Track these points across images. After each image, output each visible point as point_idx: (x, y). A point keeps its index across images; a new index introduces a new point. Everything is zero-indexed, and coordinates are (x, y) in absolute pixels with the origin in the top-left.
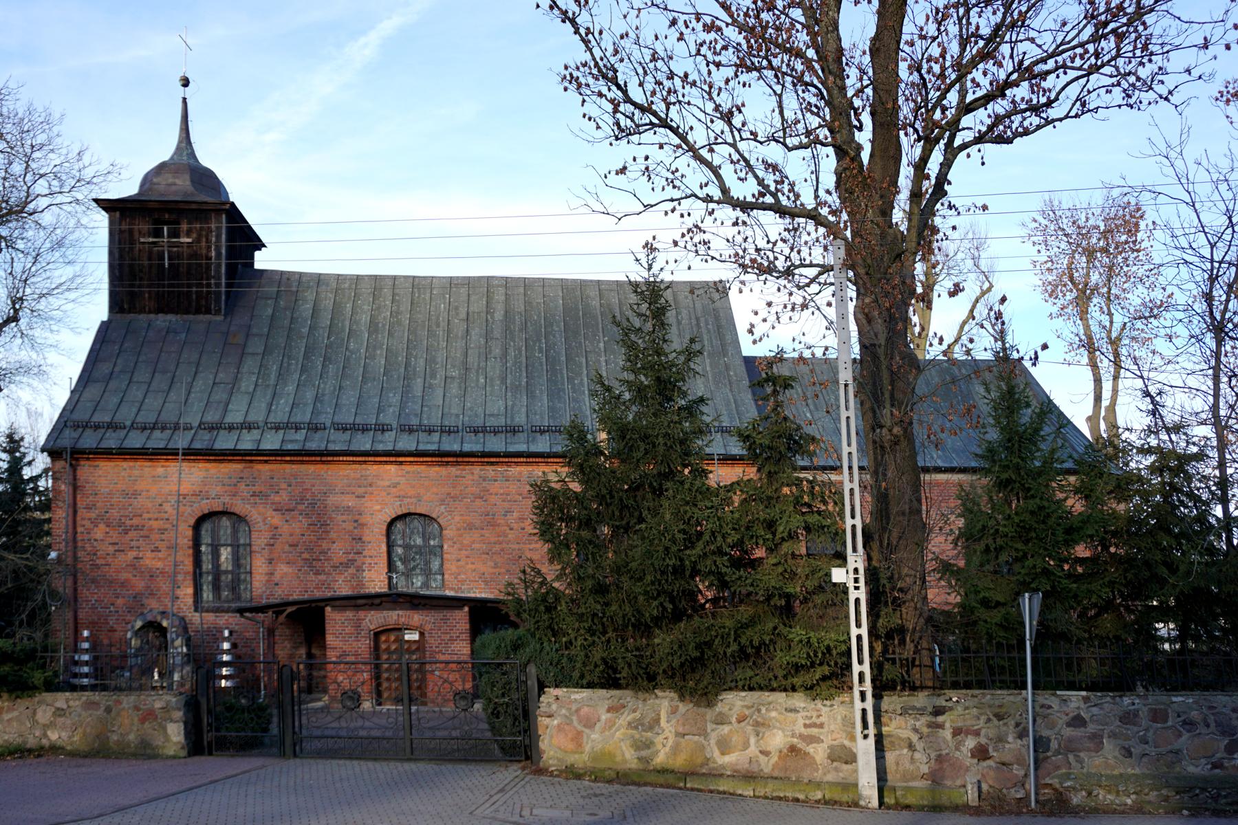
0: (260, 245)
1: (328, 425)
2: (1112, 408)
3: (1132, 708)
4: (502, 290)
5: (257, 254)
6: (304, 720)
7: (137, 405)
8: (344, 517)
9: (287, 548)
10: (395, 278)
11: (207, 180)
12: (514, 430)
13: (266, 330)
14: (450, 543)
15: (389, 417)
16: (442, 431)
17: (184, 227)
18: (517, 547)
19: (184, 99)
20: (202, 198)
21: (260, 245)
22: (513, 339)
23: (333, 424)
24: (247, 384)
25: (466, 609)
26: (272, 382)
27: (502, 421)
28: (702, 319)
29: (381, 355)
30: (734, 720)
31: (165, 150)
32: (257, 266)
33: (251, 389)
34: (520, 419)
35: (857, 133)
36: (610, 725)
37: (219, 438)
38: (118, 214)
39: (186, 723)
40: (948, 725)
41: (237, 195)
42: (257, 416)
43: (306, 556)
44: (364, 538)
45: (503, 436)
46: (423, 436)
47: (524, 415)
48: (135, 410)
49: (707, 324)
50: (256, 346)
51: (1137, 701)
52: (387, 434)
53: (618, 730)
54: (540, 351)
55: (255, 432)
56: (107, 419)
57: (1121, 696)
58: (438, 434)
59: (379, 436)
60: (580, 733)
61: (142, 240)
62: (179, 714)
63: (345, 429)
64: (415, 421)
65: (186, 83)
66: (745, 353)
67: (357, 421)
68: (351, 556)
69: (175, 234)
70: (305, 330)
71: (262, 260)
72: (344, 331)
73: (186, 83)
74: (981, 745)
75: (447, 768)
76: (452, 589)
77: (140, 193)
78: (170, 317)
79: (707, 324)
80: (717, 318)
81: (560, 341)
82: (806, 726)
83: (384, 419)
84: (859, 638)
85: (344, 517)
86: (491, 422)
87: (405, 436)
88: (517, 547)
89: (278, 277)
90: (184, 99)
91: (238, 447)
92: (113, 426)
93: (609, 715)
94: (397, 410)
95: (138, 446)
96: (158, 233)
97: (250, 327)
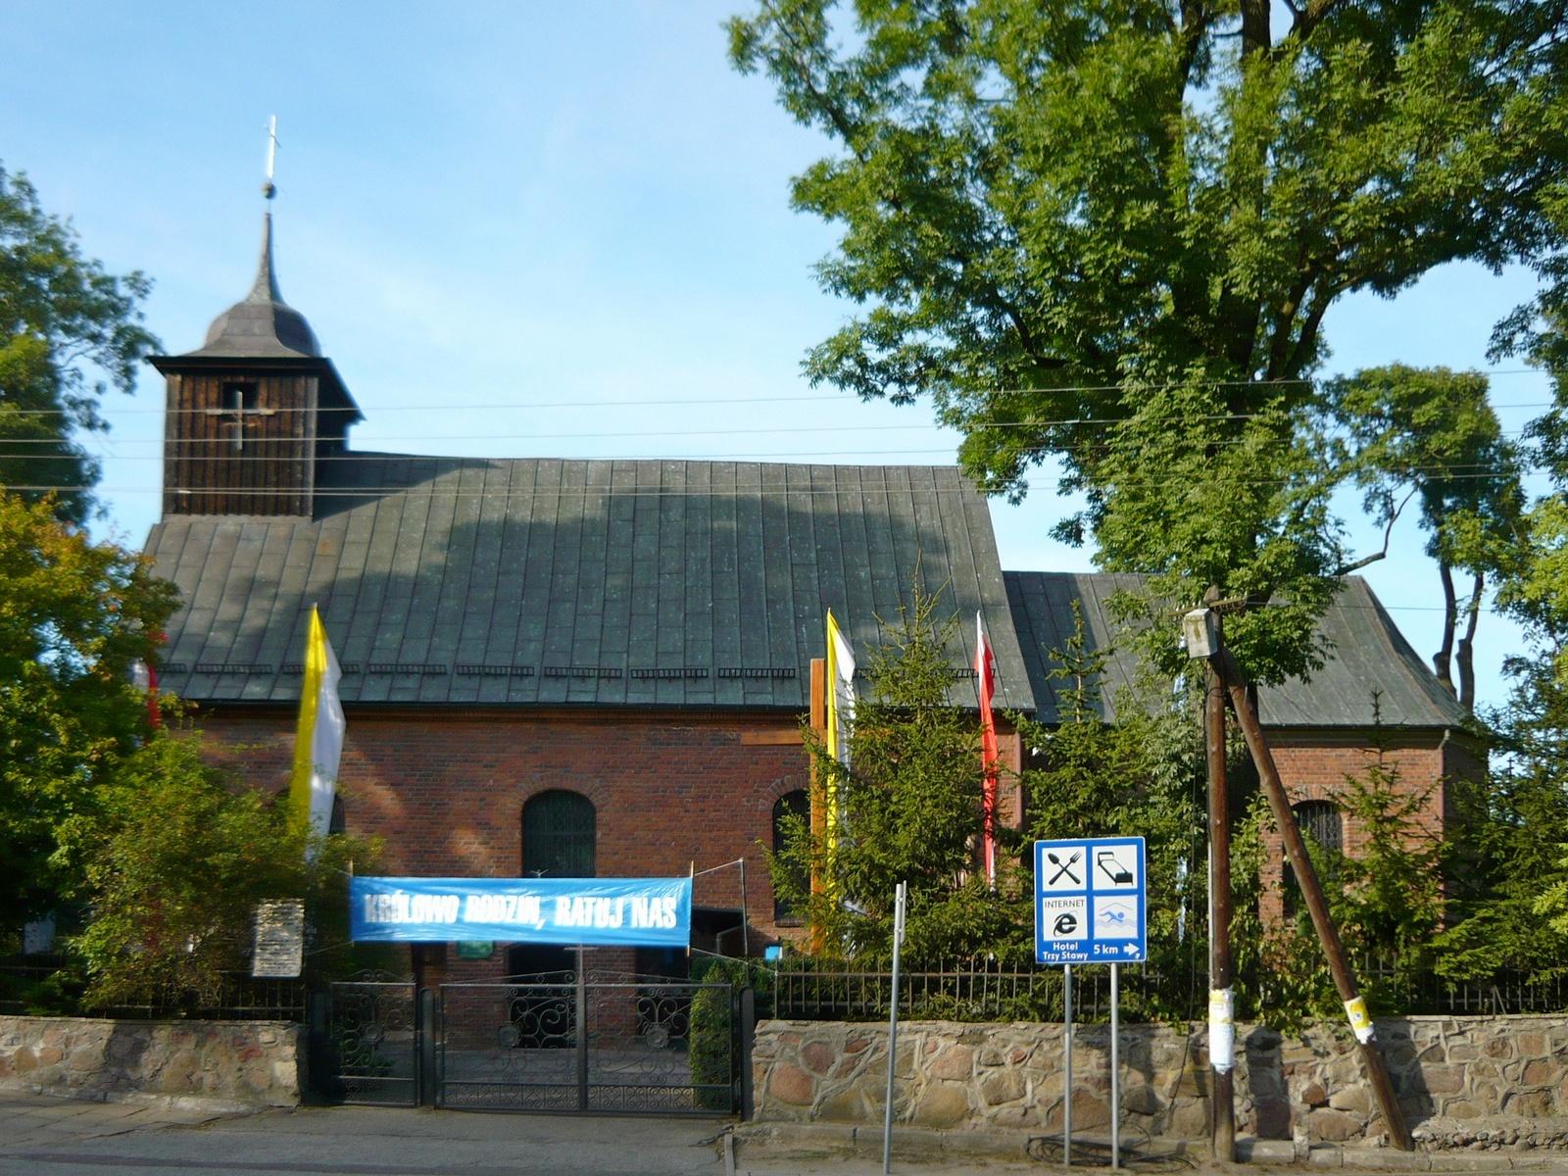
0: (354, 416)
1: (449, 669)
2: (1466, 646)
10: (537, 461)
11: (291, 327)
12: (695, 676)
15: (529, 656)
16: (599, 677)
17: (263, 393)
20: (291, 353)
21: (354, 416)
23: (456, 666)
28: (948, 520)
30: (1008, 1061)
31: (239, 285)
33: (347, 618)
34: (703, 659)
38: (179, 378)
39: (298, 1062)
41: (330, 346)
44: (493, 823)
45: (681, 683)
46: (576, 685)
47: (708, 654)
49: (954, 526)
52: (526, 681)
55: (355, 677)
60: (807, 1079)
62: (290, 1050)
63: (470, 675)
64: (562, 662)
65: (271, 192)
66: (1006, 566)
69: (249, 402)
70: (418, 536)
73: (271, 192)
77: (205, 348)
78: (244, 518)
79: (954, 526)
80: (968, 518)
83: (523, 659)
86: (666, 664)
87: (551, 683)
91: (273, 697)
93: (847, 1055)
95: (233, 697)
96: (228, 402)
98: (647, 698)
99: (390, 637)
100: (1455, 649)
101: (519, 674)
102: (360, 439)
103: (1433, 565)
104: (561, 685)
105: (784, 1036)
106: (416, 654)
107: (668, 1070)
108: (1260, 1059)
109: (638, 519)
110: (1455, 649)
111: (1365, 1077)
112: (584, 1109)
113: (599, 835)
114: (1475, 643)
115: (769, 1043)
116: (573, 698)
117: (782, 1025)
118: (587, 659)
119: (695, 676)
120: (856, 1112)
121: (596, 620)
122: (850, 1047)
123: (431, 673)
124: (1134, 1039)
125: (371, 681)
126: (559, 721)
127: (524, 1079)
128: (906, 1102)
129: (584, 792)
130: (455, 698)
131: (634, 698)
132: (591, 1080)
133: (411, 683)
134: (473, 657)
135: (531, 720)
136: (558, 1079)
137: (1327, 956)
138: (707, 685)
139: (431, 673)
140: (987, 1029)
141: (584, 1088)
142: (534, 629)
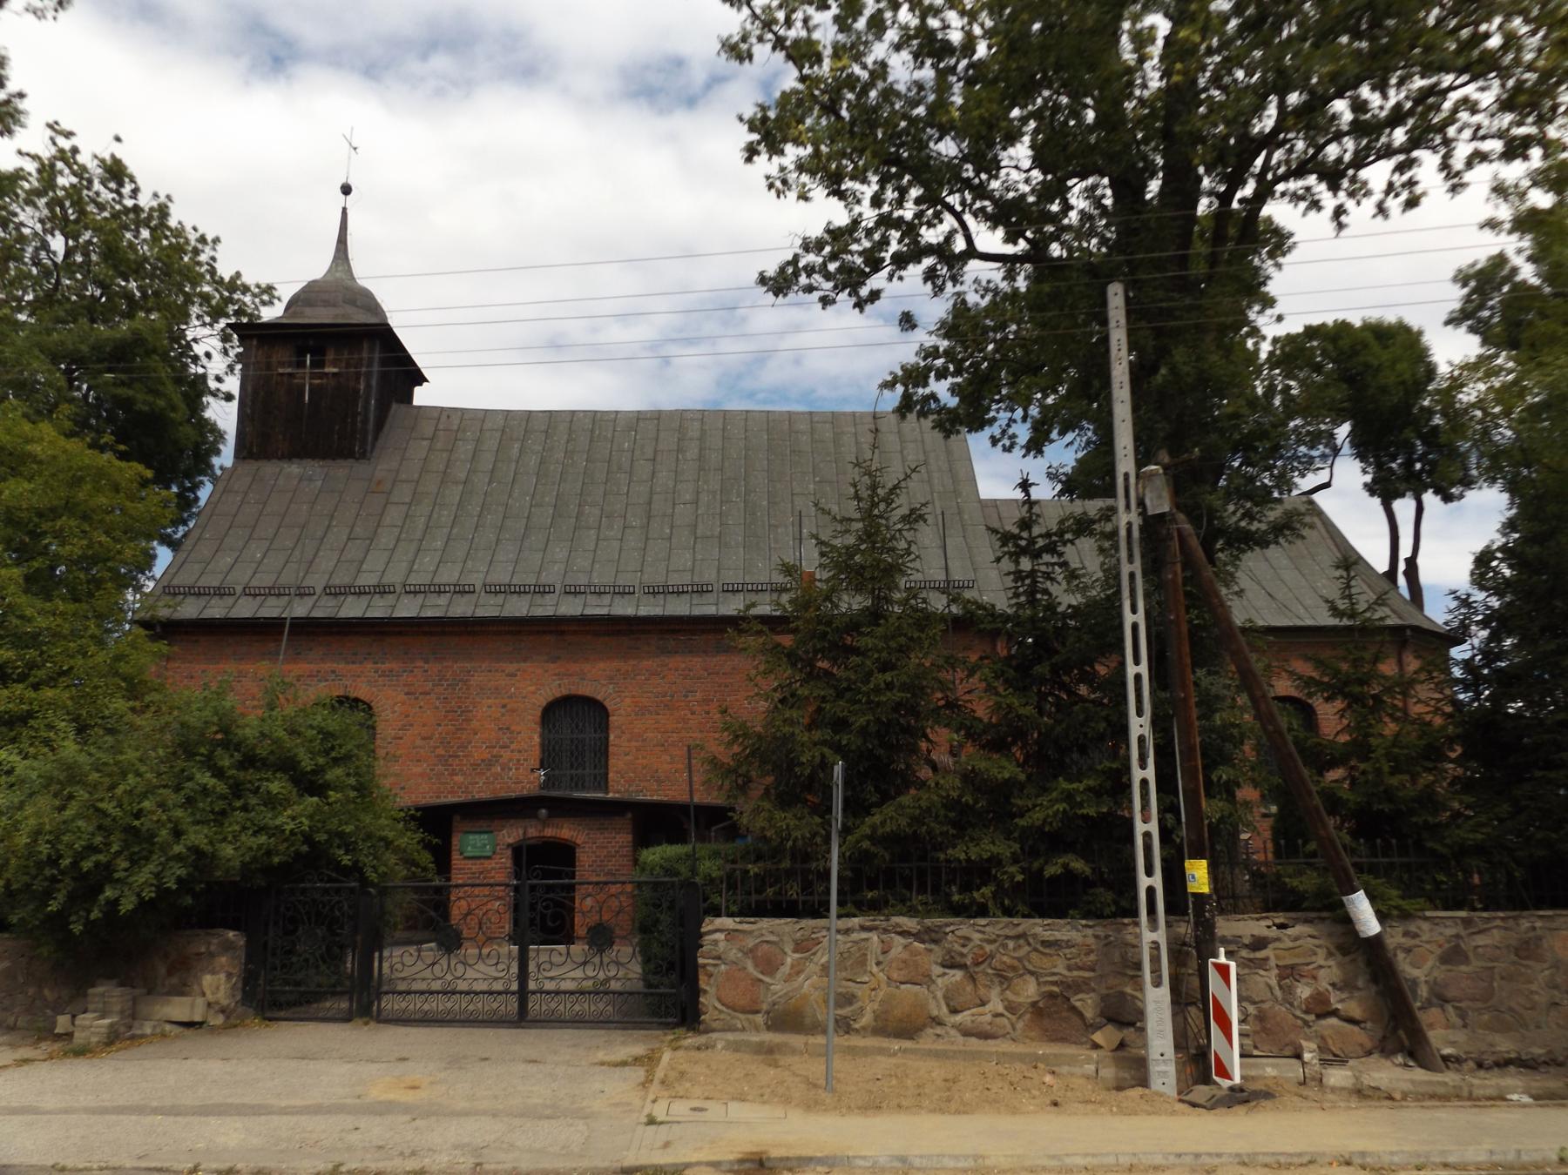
0: (420, 379)
2: (1412, 563)
3: (1531, 934)
4: (697, 425)
5: (417, 390)
7: (254, 565)
9: (419, 742)
11: (367, 301)
13: (416, 476)
17: (330, 356)
18: (699, 735)
19: (344, 210)
21: (420, 379)
24: (386, 539)
25: (629, 815)
26: (418, 535)
27: (687, 579)
31: (316, 266)
32: (416, 402)
34: (709, 575)
36: (797, 971)
37: (346, 604)
40: (1273, 962)
42: (394, 577)
45: (686, 597)
46: (592, 599)
48: (250, 573)
50: (403, 493)
51: (1538, 924)
52: (547, 597)
54: (738, 496)
56: (216, 584)
57: (1515, 918)
58: (608, 597)
59: (538, 599)
65: (346, 190)
67: (515, 581)
68: (495, 751)
71: (422, 396)
73: (346, 190)
74: (1319, 993)
82: (1069, 968)
84: (1135, 627)
86: (675, 580)
88: (699, 735)
89: (436, 415)
90: (344, 210)
92: (220, 592)
93: (797, 956)
94: (563, 567)
97: (398, 472)
98: (657, 611)
99: (428, 561)
100: (1402, 566)
101: (543, 590)
102: (227, 279)
103: (1377, 501)
104: (579, 600)
105: (731, 934)
106: (449, 575)
107: (612, 974)
108: (1250, 960)
109: (659, 458)
110: (1402, 566)
111: (980, 839)
112: (522, 1019)
113: (612, 737)
114: (1420, 561)
115: (716, 942)
116: (588, 611)
117: (728, 922)
118: (602, 577)
119: (701, 590)
120: (808, 1021)
121: (616, 544)
122: (799, 947)
123: (462, 591)
124: (1107, 937)
125: (406, 600)
126: (575, 633)
127: (462, 986)
128: (862, 1009)
129: (599, 697)
130: (480, 613)
131: (644, 611)
132: (532, 985)
133: (443, 600)
134: (501, 576)
135: (551, 632)
136: (498, 986)
137: (845, 105)
138: (711, 598)
139: (462, 591)
140: (947, 925)
141: (523, 994)
142: (559, 552)
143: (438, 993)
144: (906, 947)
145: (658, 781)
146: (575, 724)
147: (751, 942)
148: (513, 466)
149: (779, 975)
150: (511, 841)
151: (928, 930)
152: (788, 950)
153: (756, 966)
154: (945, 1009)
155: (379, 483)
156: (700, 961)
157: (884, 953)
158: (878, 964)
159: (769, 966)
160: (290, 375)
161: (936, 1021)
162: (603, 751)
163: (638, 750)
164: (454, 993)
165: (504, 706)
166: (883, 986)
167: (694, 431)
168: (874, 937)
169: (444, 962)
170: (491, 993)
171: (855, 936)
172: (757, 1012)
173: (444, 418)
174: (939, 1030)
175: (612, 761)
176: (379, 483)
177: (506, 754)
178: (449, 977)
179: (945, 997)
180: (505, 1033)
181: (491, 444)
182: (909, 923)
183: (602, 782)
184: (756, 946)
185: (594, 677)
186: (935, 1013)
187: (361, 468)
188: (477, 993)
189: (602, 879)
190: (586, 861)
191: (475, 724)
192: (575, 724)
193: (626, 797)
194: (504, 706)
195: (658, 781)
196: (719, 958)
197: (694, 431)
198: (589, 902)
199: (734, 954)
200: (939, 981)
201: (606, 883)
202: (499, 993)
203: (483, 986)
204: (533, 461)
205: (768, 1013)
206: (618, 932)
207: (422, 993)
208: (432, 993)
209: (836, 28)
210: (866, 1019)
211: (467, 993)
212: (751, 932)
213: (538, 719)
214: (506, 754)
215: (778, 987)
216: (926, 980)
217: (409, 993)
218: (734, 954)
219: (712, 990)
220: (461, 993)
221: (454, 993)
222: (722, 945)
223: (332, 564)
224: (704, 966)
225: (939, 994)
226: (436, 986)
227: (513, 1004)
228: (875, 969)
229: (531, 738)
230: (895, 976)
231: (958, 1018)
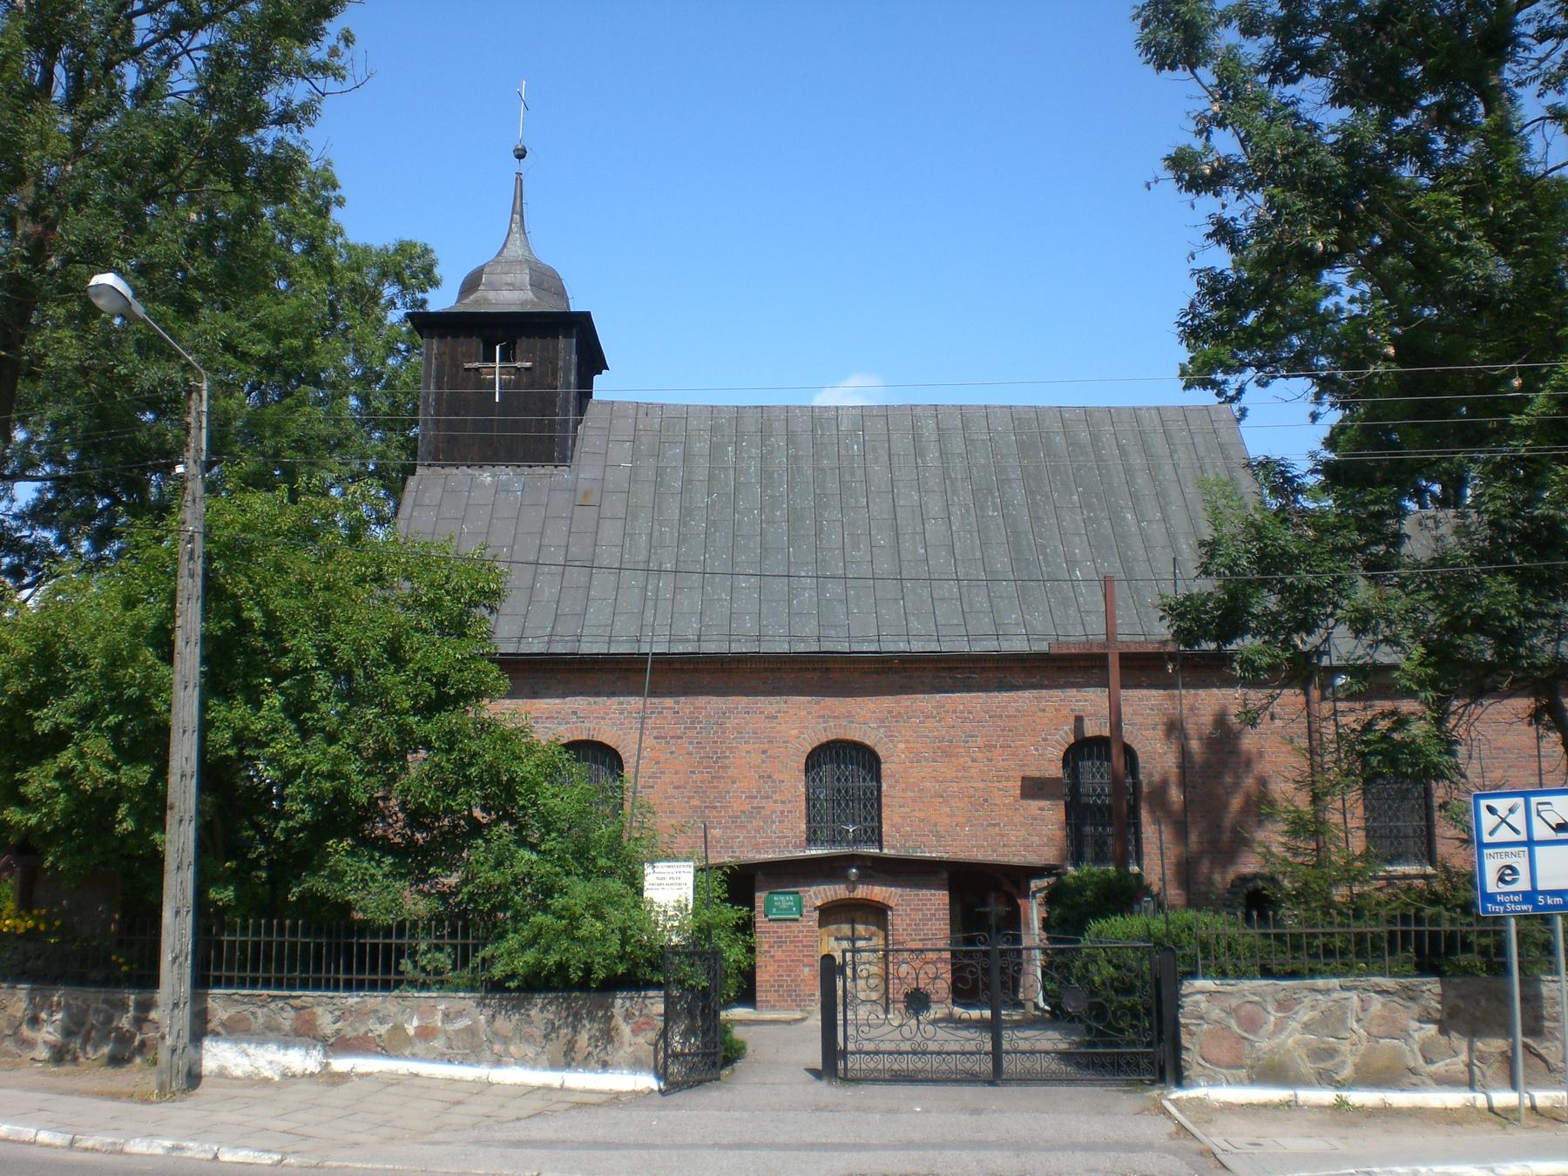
4: (931, 423)
6: (851, 1030)
8: (749, 747)
9: (670, 790)
14: (891, 781)
22: (955, 492)
28: (1207, 460)
29: (1452, 921)
35: (1524, 704)
36: (1280, 1027)
43: (696, 802)
53: (1290, 1036)
61: (467, 366)
65: (521, 154)
68: (756, 803)
72: (727, 485)
75: (1089, 1075)
76: (893, 847)
81: (1018, 494)
85: (749, 747)
88: (982, 785)
112: (996, 1077)
115: (1197, 1003)
120: (1292, 1074)
122: (1282, 1006)
127: (932, 1046)
128: (1344, 1062)
129: (867, 742)
141: (997, 1054)
143: (907, 1053)
144: (1384, 1005)
145: (939, 836)
146: (845, 768)
147: (1234, 1002)
148: (731, 472)
149: (1262, 1032)
150: (819, 903)
151: (1406, 988)
152: (1270, 1009)
153: (1240, 1025)
154: (1421, 1060)
155: (586, 494)
156: (1182, 1021)
157: (1364, 1010)
158: (1359, 1020)
159: (1252, 1024)
160: (477, 369)
161: (1413, 1071)
162: (874, 803)
163: (914, 801)
164: (924, 1053)
165: (764, 752)
166: (1364, 1042)
167: (929, 428)
168: (1353, 996)
169: (913, 1022)
170: (963, 1053)
171: (1335, 995)
172: (1242, 1067)
173: (641, 414)
174: (1414, 1079)
175: (885, 813)
176: (586, 494)
177: (769, 805)
178: (919, 1038)
179: (1421, 1050)
180: (969, 1093)
181: (701, 446)
182: (1388, 983)
183: (877, 837)
184: (1239, 1006)
185: (860, 717)
186: (1412, 1064)
187: (563, 474)
188: (948, 1054)
189: (920, 945)
190: (899, 921)
191: (732, 771)
192: (845, 768)
193: (903, 853)
194: (764, 752)
195: (939, 836)
196: (1201, 1018)
197: (929, 428)
198: (904, 968)
199: (1216, 1013)
200: (1416, 1035)
201: (922, 951)
202: (972, 1053)
203: (957, 1047)
204: (754, 467)
205: (1252, 1067)
206: (934, 997)
207: (891, 1053)
208: (900, 1053)
209: (1182, 73)
210: (1347, 1072)
211: (938, 1053)
212: (1232, 994)
213: (803, 767)
214: (769, 805)
215: (1264, 1044)
216: (1405, 1034)
217: (876, 1053)
218: (1216, 1013)
219: (1195, 1048)
220: (932, 1053)
221: (924, 1053)
222: (1203, 1006)
223: (555, 590)
224: (1186, 1026)
225: (1416, 1047)
226: (906, 1046)
227: (986, 1065)
228: (1355, 1026)
229: (796, 787)
230: (1374, 1031)
231: (1432, 1068)
